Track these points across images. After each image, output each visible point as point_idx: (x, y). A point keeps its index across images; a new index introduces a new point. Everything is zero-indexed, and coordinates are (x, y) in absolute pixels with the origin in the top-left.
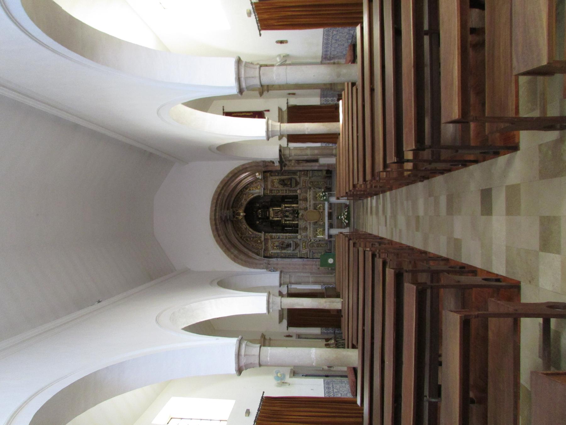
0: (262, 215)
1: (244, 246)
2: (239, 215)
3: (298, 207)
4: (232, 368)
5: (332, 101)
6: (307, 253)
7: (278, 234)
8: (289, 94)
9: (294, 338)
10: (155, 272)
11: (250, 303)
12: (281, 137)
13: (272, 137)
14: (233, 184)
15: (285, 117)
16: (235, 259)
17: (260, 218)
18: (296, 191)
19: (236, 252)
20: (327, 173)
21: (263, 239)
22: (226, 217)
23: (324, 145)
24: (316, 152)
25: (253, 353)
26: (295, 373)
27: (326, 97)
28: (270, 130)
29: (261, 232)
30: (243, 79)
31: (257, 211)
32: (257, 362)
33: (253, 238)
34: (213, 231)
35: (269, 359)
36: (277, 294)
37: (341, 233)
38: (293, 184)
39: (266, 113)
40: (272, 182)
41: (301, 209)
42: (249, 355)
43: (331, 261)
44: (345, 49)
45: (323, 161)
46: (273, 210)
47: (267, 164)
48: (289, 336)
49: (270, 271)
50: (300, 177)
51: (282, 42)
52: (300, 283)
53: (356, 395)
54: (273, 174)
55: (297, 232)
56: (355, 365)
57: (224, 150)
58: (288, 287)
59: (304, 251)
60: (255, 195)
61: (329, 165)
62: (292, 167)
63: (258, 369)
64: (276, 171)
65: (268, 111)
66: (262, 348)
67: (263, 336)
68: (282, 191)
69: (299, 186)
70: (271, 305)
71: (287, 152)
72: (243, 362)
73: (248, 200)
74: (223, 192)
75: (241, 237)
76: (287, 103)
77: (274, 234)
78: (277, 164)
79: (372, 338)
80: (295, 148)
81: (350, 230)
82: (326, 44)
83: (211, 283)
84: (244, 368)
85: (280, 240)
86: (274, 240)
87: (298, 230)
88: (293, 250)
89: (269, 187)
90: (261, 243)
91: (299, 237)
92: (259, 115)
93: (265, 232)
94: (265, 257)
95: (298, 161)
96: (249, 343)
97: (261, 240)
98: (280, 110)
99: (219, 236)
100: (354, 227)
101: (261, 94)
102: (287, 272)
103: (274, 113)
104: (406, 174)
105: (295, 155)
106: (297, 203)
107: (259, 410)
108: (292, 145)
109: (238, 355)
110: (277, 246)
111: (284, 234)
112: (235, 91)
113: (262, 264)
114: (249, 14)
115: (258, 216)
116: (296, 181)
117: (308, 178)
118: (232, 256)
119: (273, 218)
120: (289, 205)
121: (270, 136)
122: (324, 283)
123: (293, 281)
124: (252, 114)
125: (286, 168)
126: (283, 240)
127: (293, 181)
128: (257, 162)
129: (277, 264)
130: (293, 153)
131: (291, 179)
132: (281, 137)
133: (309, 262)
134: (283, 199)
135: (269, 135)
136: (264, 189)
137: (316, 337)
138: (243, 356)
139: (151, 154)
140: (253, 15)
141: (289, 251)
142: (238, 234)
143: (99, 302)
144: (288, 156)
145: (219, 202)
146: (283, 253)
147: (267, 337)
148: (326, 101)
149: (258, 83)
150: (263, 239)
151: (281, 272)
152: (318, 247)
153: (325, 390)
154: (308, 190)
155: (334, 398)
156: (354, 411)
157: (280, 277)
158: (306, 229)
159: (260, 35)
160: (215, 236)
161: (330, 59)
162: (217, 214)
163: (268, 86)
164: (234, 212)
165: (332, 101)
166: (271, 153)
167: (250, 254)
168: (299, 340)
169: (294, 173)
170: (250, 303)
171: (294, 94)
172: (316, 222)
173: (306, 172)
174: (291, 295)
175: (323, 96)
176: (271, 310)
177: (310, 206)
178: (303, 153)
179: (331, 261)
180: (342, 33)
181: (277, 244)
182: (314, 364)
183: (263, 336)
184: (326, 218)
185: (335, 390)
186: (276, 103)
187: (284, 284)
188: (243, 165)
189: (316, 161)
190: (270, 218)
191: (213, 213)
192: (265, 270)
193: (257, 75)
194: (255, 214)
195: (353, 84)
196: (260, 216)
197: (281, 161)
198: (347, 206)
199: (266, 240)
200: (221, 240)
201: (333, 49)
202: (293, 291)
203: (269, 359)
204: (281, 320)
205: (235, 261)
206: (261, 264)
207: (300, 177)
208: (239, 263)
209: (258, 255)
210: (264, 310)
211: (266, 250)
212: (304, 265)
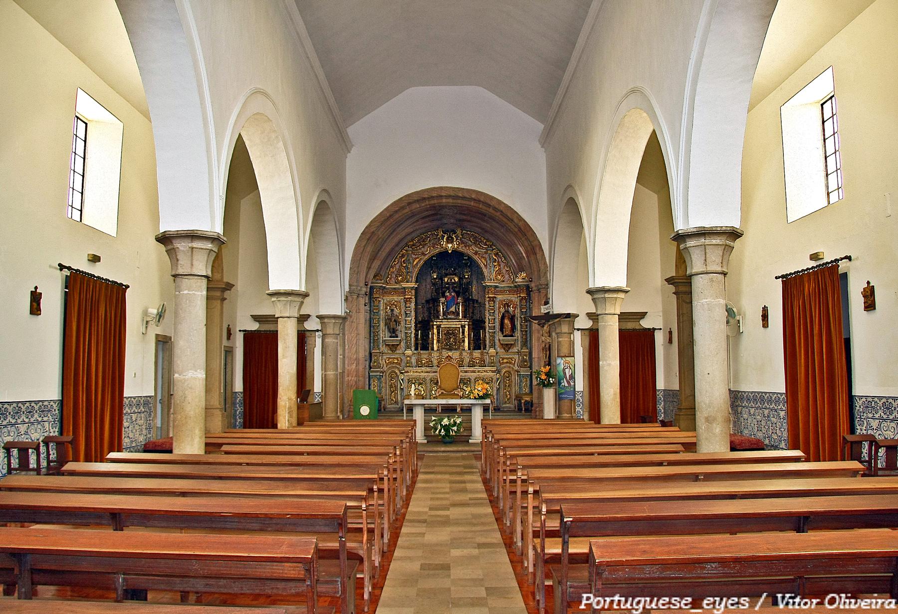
0: (447, 283)
2: (448, 242)
4: (168, 225)
8: (670, 333)
9: (225, 342)
12: (593, 316)
15: (630, 325)
16: (368, 235)
17: (442, 280)
18: (493, 346)
20: (526, 402)
21: (404, 285)
28: (607, 295)
29: (416, 282)
30: (702, 241)
31: (455, 274)
32: (180, 271)
33: (407, 268)
35: (186, 292)
36: (304, 312)
37: (415, 424)
42: (192, 255)
44: (751, 431)
47: (543, 291)
48: (229, 334)
50: (518, 353)
51: (765, 317)
52: (324, 353)
53: (145, 451)
55: (416, 349)
56: (176, 451)
57: (569, 211)
58: (318, 331)
60: (484, 270)
61: (541, 404)
63: (169, 272)
66: (205, 281)
68: (492, 319)
69: (501, 351)
71: (565, 328)
72: (182, 246)
73: (476, 257)
75: (406, 245)
77: (413, 305)
78: (544, 310)
79: (184, 494)
80: (572, 344)
81: (422, 444)
82: (760, 398)
84: (170, 247)
85: (402, 318)
86: (403, 304)
89: (499, 297)
91: (409, 352)
96: (213, 255)
98: (643, 315)
99: (409, 204)
101: (669, 281)
102: (344, 329)
109: (193, 236)
110: (392, 310)
111: (413, 325)
112: (680, 226)
114: (814, 257)
115: (446, 275)
117: (516, 368)
119: (439, 327)
120: (466, 334)
121: (595, 296)
122: (324, 396)
126: (403, 323)
128: (545, 273)
130: (564, 340)
132: (593, 316)
133: (363, 365)
134: (477, 325)
136: (496, 287)
138: (190, 245)
140: (814, 264)
141: (384, 334)
144: (558, 331)
147: (227, 294)
149: (694, 271)
150: (404, 285)
152: (391, 386)
153: (134, 398)
154: (494, 369)
159: (776, 278)
162: (451, 200)
166: (564, 299)
169: (526, 343)
171: (670, 341)
172: (437, 383)
174: (302, 338)
175: (669, 394)
177: (466, 372)
179: (365, 410)
180: (778, 425)
181: (396, 311)
182: (176, 375)
184: (443, 402)
185: (134, 416)
192: (347, 289)
194: (451, 262)
195: (690, 447)
196: (446, 280)
197: (549, 318)
201: (752, 411)
202: (309, 341)
203: (186, 292)
204: (256, 318)
209: (375, 277)
212: (357, 359)
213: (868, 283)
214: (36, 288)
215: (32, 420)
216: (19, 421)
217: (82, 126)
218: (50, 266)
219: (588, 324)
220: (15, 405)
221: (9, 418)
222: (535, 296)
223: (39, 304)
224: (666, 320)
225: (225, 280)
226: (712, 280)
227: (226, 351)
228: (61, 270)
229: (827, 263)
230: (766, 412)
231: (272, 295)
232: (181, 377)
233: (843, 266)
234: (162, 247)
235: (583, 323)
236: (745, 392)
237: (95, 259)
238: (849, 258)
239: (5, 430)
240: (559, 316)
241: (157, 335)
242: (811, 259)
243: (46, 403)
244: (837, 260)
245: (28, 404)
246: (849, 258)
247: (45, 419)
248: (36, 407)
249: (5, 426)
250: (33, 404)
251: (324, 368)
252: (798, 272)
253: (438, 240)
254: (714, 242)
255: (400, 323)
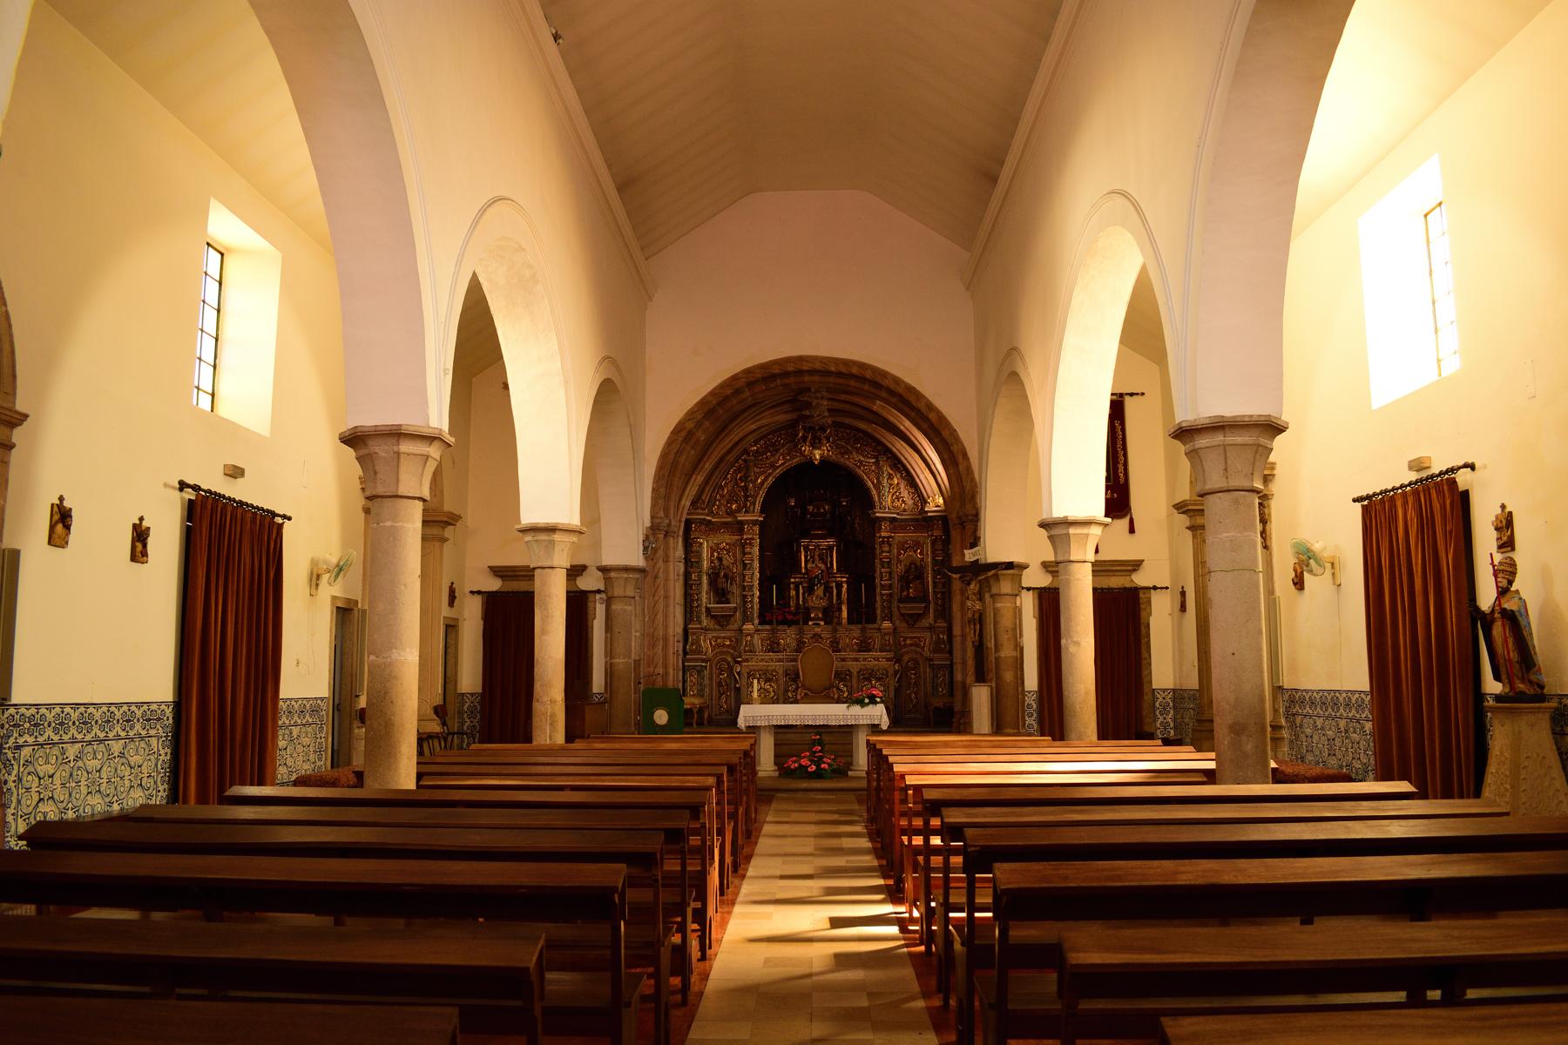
0: (812, 514)
1: (721, 459)
2: (814, 446)
3: (839, 623)
5: (1165, 725)
6: (700, 652)
7: (756, 564)
8: (1183, 594)
9: (445, 611)
10: (642, 201)
11: (549, 468)
12: (1050, 567)
13: (1051, 538)
14: (906, 425)
15: (1115, 582)
19: (702, 436)
22: (808, 405)
23: (1031, 700)
24: (1008, 676)
25: (403, 477)
26: (345, 614)
27: (1175, 708)
28: (1072, 531)
29: (762, 511)
30: (1218, 438)
32: (380, 490)
33: (746, 488)
34: (762, 366)
35: (388, 524)
38: (909, 608)
39: (1124, 523)
40: (918, 544)
41: (835, 631)
43: (661, 717)
45: (981, 697)
46: (830, 548)
47: (969, 526)
49: (647, 538)
50: (931, 628)
52: (609, 627)
54: (939, 546)
56: (368, 781)
58: (599, 591)
59: (706, 645)
60: (874, 492)
62: (965, 602)
64: (948, 557)
65: (1132, 530)
66: (419, 505)
67: (451, 520)
68: (885, 579)
69: (901, 625)
70: (543, 537)
71: (1006, 587)
72: (381, 449)
74: (884, 394)
75: (746, 451)
76: (1155, 588)
78: (969, 555)
80: (1018, 612)
82: (1331, 701)
83: (608, 360)
84: (364, 452)
87: (770, 623)
88: (708, 609)
89: (899, 536)
90: (731, 513)
91: (748, 627)
92: (1118, 501)
93: (762, 525)
94: (688, 523)
95: (980, 619)
97: (739, 510)
98: (1136, 565)
100: (778, 790)
101: (1181, 507)
103: (1121, 547)
104: (905, 839)
105: (996, 612)
106: (850, 621)
107: (241, 503)
108: (1028, 604)
110: (720, 559)
111: (756, 583)
113: (667, 516)
114: (1417, 465)
116: (919, 617)
117: (927, 653)
118: (690, 425)
123: (616, 607)
124: (1122, 480)
125: (957, 585)
127: (917, 608)
129: (666, 560)
131: (924, 598)
135: (1056, 528)
137: (449, 679)
139: (993, 180)
140: (1413, 476)
141: (705, 597)
142: (756, 442)
143: (556, 37)
145: (852, 383)
146: (700, 578)
147: (449, 532)
148: (1165, 707)
151: (641, 570)
152: (719, 684)
153: (296, 700)
154: (890, 655)
155: (275, 726)
156: (1554, 1018)
157: (627, 569)
158: (773, 647)
160: (748, 371)
161: (1290, 716)
162: (816, 378)
163: (1203, 527)
164: (823, 429)
165: (1165, 725)
166: (1004, 537)
167: (699, 479)
168: (442, 628)
169: (944, 612)
170: (549, 468)
171: (1183, 608)
173: (946, 646)
174: (578, 605)
175: (1178, 695)
176: (528, 538)
178: (1005, 638)
179: (661, 717)
180: (1361, 741)
183: (451, 520)
185: (295, 731)
186: (1156, 550)
187: (607, 580)
188: (965, 455)
189: (981, 678)
190: (804, 542)
191: (818, 366)
192: (648, 523)
193: (1233, 483)
194: (818, 501)
198: (842, 772)
199: (739, 527)
200: (737, 392)
201: (1319, 722)
203: (388, 524)
204: (497, 571)
205: (677, 431)
206: (666, 510)
207: (931, 628)
208: (669, 443)
210: (530, 515)
211: (711, 528)
213: (1503, 507)
214: (141, 519)
215: (131, 734)
216: (111, 735)
217: (214, 257)
218: (166, 485)
219: (1044, 581)
220: (105, 709)
221: (96, 730)
222: (955, 534)
223: (145, 546)
224: (1176, 571)
225: (447, 508)
226: (1236, 502)
227: (447, 627)
228: (181, 490)
229: (1432, 477)
230: (1342, 724)
231: (526, 531)
232: (380, 660)
233: (1463, 479)
234: (350, 452)
235: (1036, 578)
236: (1307, 691)
237: (235, 472)
238: (1472, 467)
239: (89, 749)
240: (995, 566)
241: (334, 598)
242: (1410, 468)
243: (154, 707)
244: (1453, 470)
245: (125, 708)
246: (1472, 467)
247: (153, 732)
248: (139, 713)
249: (90, 743)
250: (133, 708)
251: (610, 652)
252: (1386, 491)
253: (795, 448)
254: (1239, 440)
255: (733, 579)
